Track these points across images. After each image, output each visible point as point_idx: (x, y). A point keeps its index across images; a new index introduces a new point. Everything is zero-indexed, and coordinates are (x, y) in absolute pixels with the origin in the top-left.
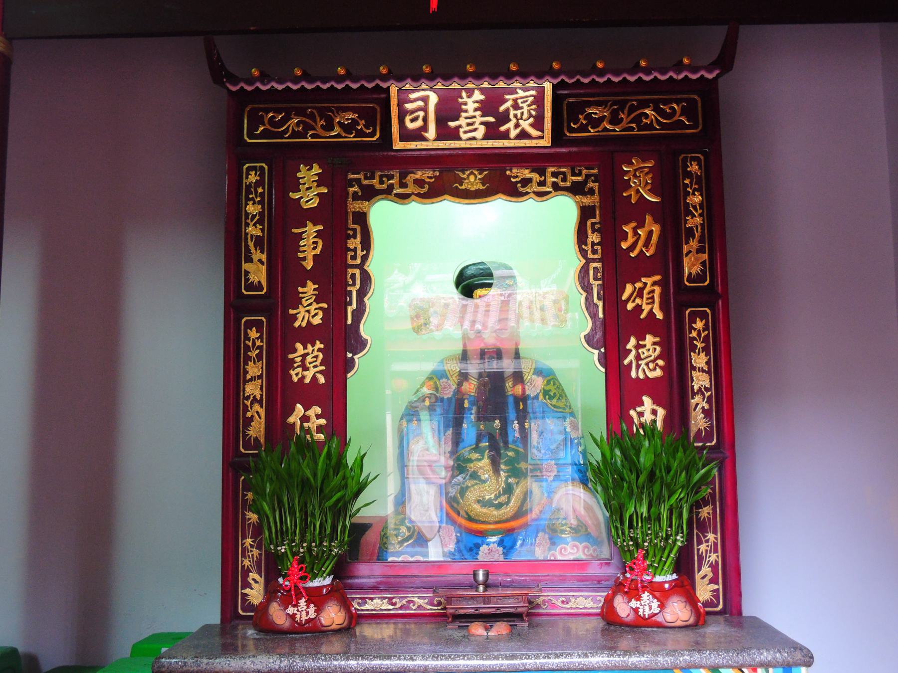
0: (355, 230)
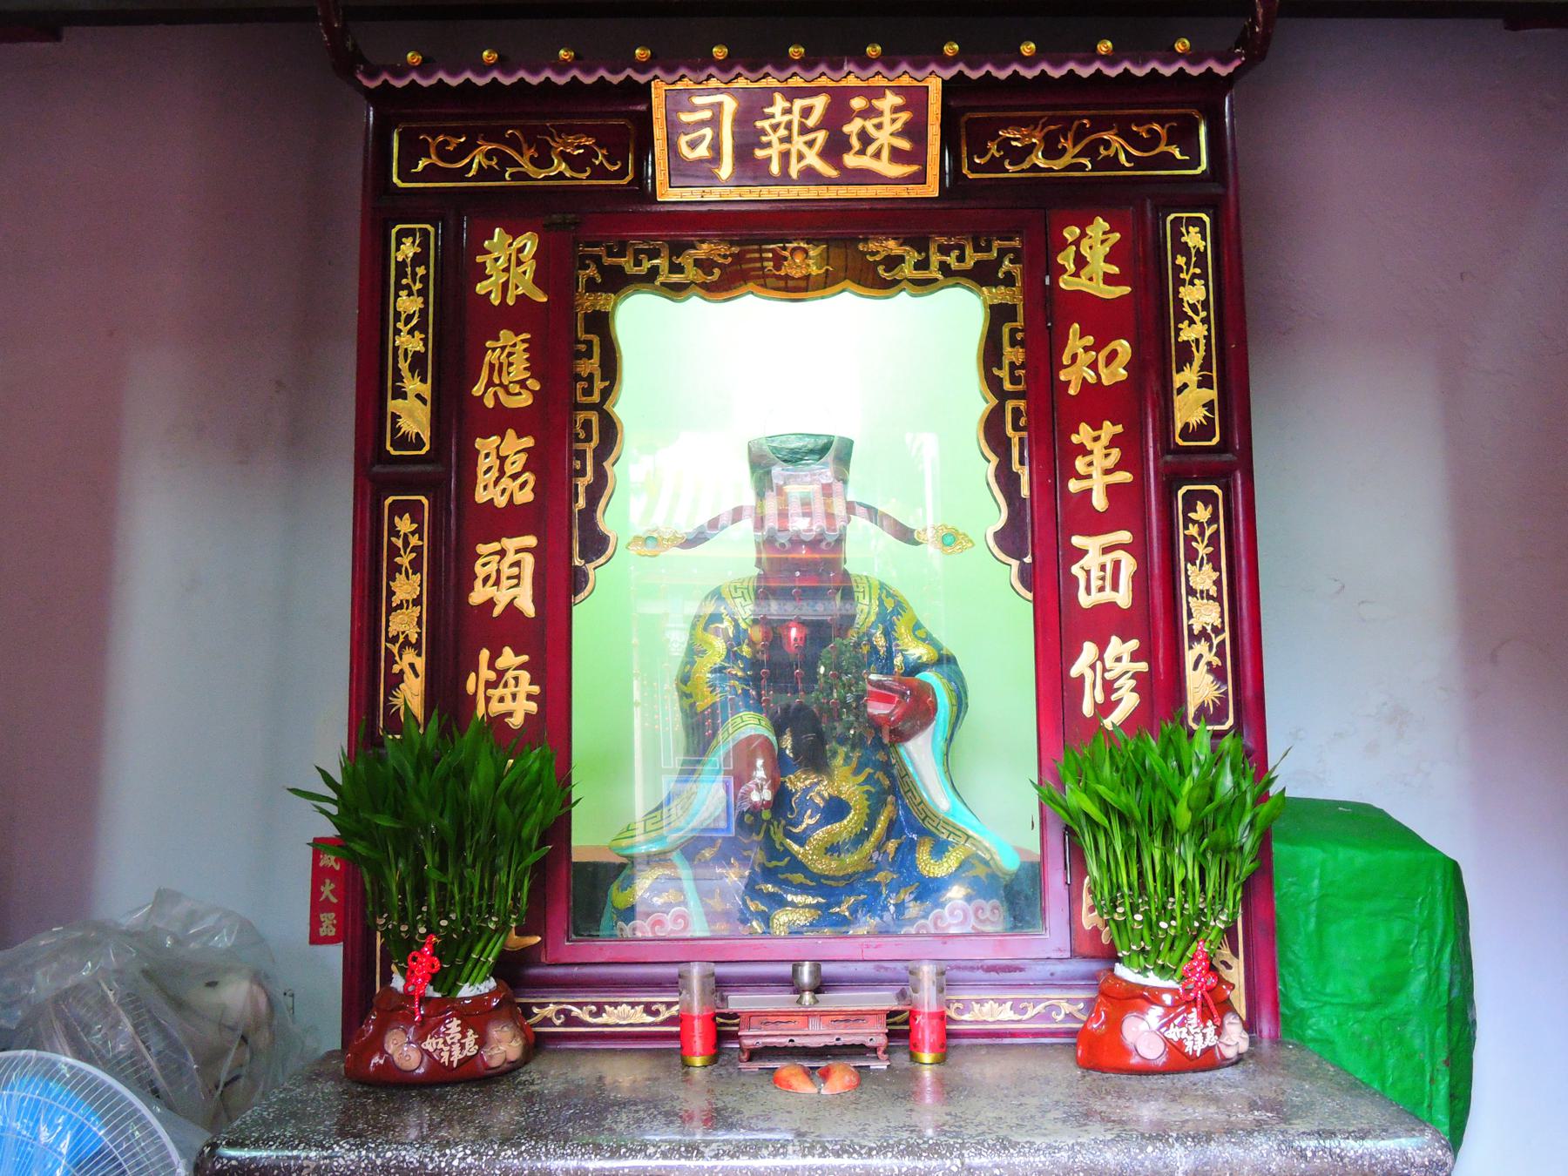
0: (589, 343)
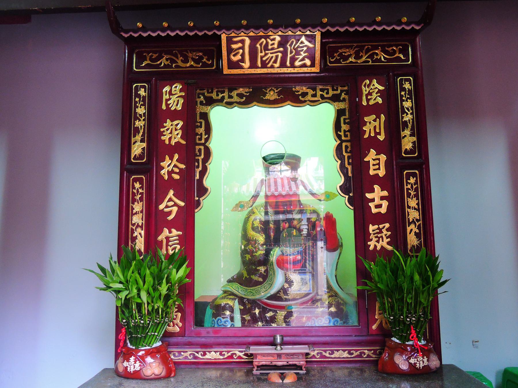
0: (201, 123)
